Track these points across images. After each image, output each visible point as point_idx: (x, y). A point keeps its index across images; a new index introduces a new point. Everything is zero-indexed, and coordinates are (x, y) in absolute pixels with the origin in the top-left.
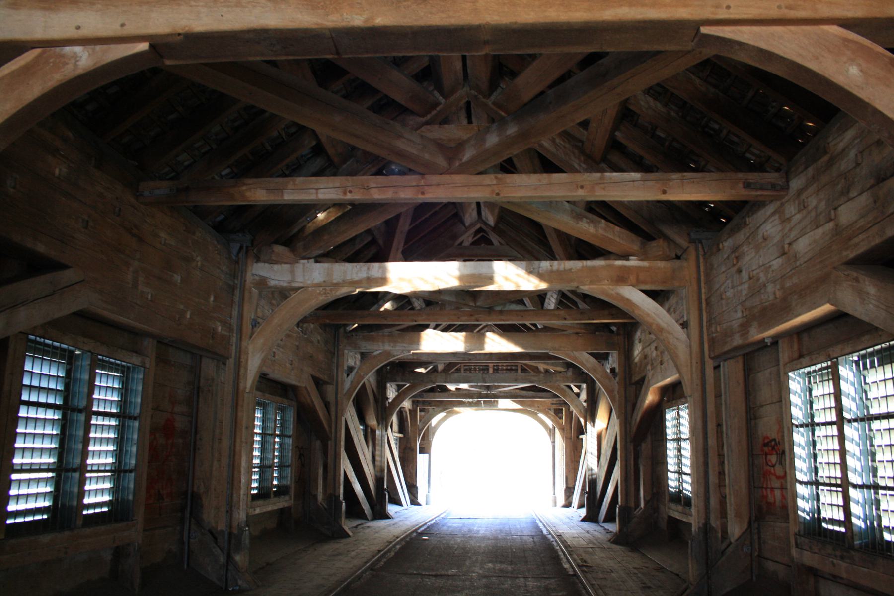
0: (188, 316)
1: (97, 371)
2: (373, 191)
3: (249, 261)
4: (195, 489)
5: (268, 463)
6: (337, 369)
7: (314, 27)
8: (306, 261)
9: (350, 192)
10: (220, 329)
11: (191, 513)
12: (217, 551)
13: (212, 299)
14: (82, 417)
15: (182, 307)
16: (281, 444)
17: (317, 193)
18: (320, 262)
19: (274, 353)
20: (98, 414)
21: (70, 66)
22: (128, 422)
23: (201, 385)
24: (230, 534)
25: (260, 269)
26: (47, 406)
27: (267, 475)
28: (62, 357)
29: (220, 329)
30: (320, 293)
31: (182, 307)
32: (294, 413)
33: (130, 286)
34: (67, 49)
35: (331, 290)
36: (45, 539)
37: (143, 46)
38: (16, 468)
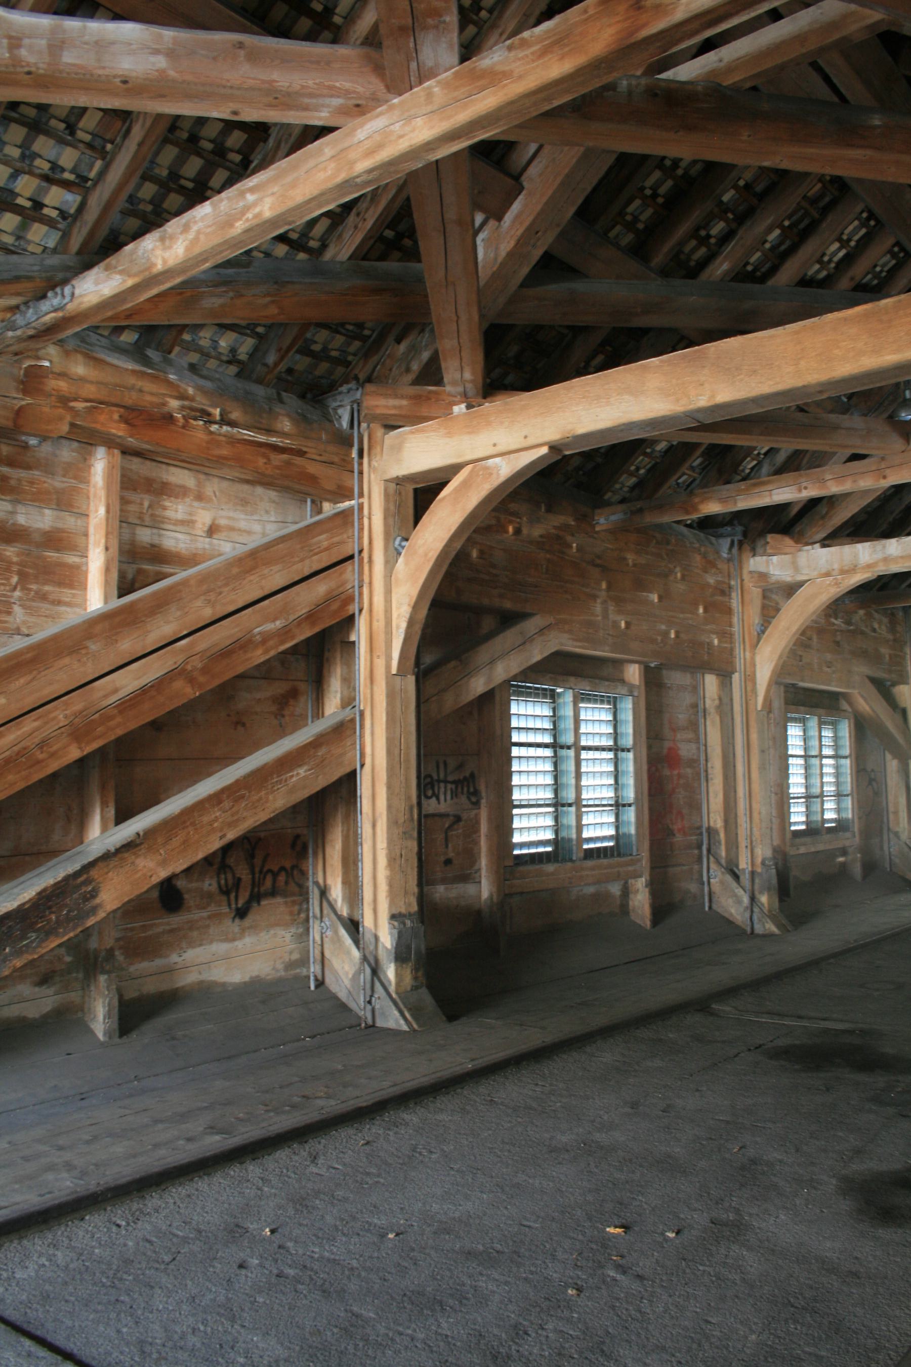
0: (673, 636)
1: (581, 705)
2: (829, 483)
3: (744, 556)
4: (712, 824)
5: (816, 791)
6: (705, 719)
7: (668, 413)
8: (810, 547)
9: (806, 488)
10: (716, 642)
11: (709, 851)
12: (740, 892)
13: (701, 610)
14: (571, 753)
15: (663, 627)
16: (837, 767)
17: (771, 495)
18: (828, 546)
19: (801, 656)
20: (589, 748)
21: (494, 476)
22: (621, 755)
23: (707, 706)
24: (753, 873)
25: (756, 563)
26: (538, 745)
27: (816, 807)
28: (545, 696)
29: (716, 642)
30: (830, 585)
31: (663, 627)
32: (850, 726)
33: (600, 618)
34: (491, 461)
35: (843, 579)
36: (550, 868)
37: (544, 450)
38: (515, 803)
